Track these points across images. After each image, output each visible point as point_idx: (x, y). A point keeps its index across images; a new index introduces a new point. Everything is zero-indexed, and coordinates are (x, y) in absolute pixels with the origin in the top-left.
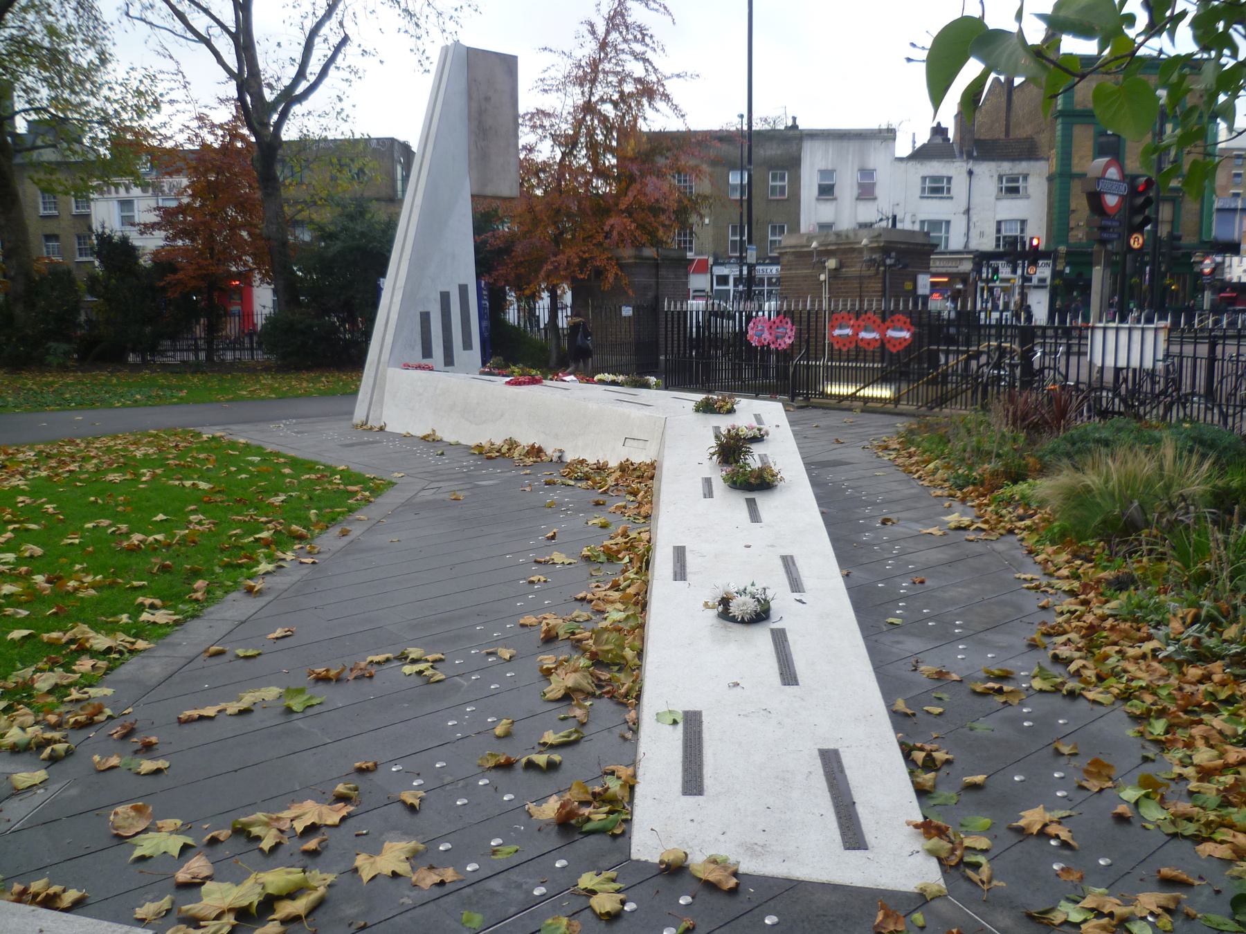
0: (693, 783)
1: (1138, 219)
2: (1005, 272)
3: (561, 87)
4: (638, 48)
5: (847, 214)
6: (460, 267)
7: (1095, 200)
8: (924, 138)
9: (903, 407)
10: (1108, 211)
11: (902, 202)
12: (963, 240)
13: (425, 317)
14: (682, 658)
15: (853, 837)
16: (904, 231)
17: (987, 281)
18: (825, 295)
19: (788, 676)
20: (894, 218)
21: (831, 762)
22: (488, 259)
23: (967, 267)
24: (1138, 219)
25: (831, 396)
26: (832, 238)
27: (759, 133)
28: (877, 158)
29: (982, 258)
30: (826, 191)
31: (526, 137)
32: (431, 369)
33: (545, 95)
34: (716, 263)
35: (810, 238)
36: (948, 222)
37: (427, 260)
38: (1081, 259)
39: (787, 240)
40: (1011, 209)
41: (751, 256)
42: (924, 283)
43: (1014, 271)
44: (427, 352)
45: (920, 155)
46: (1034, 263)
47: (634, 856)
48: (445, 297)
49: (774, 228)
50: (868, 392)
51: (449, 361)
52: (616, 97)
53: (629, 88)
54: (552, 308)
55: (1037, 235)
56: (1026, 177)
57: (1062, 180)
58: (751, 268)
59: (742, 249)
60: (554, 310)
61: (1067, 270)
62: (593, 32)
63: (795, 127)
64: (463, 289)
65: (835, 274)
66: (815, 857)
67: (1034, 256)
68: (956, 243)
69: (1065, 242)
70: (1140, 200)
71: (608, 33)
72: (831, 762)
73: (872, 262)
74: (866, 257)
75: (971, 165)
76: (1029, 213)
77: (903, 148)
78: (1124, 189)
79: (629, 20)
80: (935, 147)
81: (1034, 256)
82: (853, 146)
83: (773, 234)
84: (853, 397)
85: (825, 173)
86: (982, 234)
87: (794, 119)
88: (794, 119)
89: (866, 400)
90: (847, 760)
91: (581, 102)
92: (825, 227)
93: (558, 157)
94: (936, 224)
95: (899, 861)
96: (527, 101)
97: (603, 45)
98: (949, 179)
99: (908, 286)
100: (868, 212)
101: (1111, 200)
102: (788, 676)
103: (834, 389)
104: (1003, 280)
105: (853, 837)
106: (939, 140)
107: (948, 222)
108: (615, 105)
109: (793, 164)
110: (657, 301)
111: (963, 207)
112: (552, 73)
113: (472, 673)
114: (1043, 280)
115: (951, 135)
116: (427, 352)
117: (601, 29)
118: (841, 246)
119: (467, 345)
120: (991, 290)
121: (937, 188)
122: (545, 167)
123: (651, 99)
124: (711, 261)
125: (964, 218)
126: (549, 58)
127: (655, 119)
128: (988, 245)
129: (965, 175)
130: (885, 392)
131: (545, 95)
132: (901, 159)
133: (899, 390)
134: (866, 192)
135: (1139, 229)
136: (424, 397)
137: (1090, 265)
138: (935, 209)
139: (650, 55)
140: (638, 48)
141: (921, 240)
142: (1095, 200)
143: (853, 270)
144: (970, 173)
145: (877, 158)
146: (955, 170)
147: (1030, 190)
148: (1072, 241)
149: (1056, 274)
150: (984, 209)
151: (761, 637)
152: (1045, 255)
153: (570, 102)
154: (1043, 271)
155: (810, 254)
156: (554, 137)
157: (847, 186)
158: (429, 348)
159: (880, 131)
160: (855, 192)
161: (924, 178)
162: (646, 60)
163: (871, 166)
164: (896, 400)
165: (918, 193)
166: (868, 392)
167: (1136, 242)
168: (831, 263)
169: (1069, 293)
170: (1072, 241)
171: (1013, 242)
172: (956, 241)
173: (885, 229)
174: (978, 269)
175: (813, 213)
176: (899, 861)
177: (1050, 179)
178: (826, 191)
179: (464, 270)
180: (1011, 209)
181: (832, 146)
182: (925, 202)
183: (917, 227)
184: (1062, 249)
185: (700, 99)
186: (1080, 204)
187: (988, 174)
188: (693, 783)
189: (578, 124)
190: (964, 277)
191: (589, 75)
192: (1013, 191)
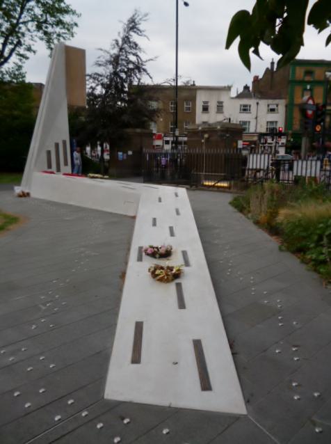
0: (136, 359)
1: (319, 119)
2: (269, 140)
3: (105, 65)
4: (134, 51)
5: (213, 118)
6: (62, 131)
7: (303, 110)
8: (241, 90)
9: (232, 190)
10: (300, 132)
11: (232, 112)
12: (254, 128)
13: (49, 153)
14: (139, 294)
15: (206, 385)
16: (233, 124)
17: (263, 144)
18: (204, 147)
19: (182, 304)
20: (230, 119)
21: (197, 345)
22: (75, 130)
23: (255, 138)
24: (319, 119)
25: (206, 186)
26: (207, 126)
27: (180, 87)
28: (224, 98)
29: (261, 135)
30: (205, 109)
31: (90, 83)
32: (52, 173)
33: (96, 66)
34: (165, 136)
35: (199, 126)
36: (249, 122)
37: (51, 129)
38: (297, 136)
39: (190, 127)
40: (272, 117)
41: (177, 133)
42: (240, 144)
43: (273, 140)
44: (50, 166)
45: (239, 96)
46: (280, 137)
47: (106, 397)
48: (57, 145)
49: (186, 123)
50: (219, 184)
51: (58, 170)
52: (126, 70)
53: (131, 66)
54: (100, 151)
55: (281, 126)
56: (277, 106)
57: (289, 108)
58: (177, 137)
59: (174, 131)
60: (103, 151)
61: (292, 140)
62: (117, 44)
63: (194, 85)
64: (64, 142)
65: (207, 140)
66: (190, 397)
67: (280, 134)
68: (252, 130)
69: (291, 130)
70: (320, 112)
71: (123, 44)
72: (197, 345)
73: (222, 136)
74: (219, 134)
75: (258, 101)
76: (279, 119)
77: (233, 94)
78: (314, 108)
79: (131, 40)
80: (246, 93)
81: (280, 134)
82: (216, 92)
83: (186, 125)
84: (213, 186)
85: (206, 102)
86: (261, 126)
87: (194, 82)
88: (194, 82)
89: (218, 187)
90: (204, 344)
91: (112, 71)
92: (204, 123)
93: (104, 92)
94: (245, 123)
95: (227, 396)
96: (90, 69)
97: (121, 49)
98: (250, 106)
99: (235, 145)
100: (220, 118)
101: (310, 112)
102: (182, 304)
103: (207, 183)
104: (269, 144)
105: (206, 385)
106: (246, 91)
107: (249, 122)
108: (126, 73)
109: (193, 99)
110: (141, 148)
111: (254, 116)
112: (102, 59)
113: (48, 302)
114: (282, 143)
115: (251, 89)
116: (50, 166)
117: (120, 43)
118: (210, 129)
119: (66, 164)
120: (264, 147)
121: (245, 109)
122: (100, 96)
123: (140, 72)
124: (163, 135)
125: (255, 121)
126: (101, 53)
127: (146, 80)
128: (264, 130)
129: (256, 104)
130: (225, 184)
131: (96, 66)
132: (233, 98)
133: (230, 184)
134: (220, 107)
135: (319, 123)
136: (47, 183)
137: (301, 138)
138: (244, 117)
139: (139, 54)
140: (134, 51)
141: (239, 127)
142: (303, 110)
143: (214, 138)
144: (258, 104)
145: (224, 98)
146: (252, 102)
147: (279, 111)
148: (294, 129)
149: (287, 141)
150: (263, 117)
151: (172, 287)
152: (284, 134)
153: (108, 71)
154: (283, 140)
155: (198, 132)
156: (102, 85)
157: (213, 106)
158: (51, 166)
159: (225, 87)
160: (216, 110)
161: (241, 105)
162: (137, 56)
163: (222, 100)
164: (229, 188)
165: (239, 110)
166: (219, 184)
167: (318, 128)
168: (206, 136)
169: (293, 148)
170: (294, 129)
171: (273, 129)
172: (252, 130)
173: (226, 123)
174: (260, 139)
175: (201, 118)
176: (227, 396)
177: (286, 106)
178: (205, 109)
179: (65, 135)
180: (272, 117)
181: (208, 93)
182: (242, 114)
183: (238, 123)
184: (290, 132)
185: (158, 74)
186: (297, 115)
187: (264, 104)
188: (136, 359)
189: (111, 80)
190: (254, 143)
191: (115, 61)
192: (272, 110)
